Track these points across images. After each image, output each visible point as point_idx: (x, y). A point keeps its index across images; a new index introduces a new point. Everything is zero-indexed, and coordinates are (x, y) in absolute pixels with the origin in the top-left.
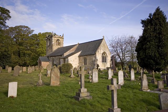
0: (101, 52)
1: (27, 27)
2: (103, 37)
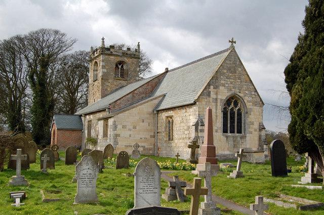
0: (219, 97)
2: (232, 42)
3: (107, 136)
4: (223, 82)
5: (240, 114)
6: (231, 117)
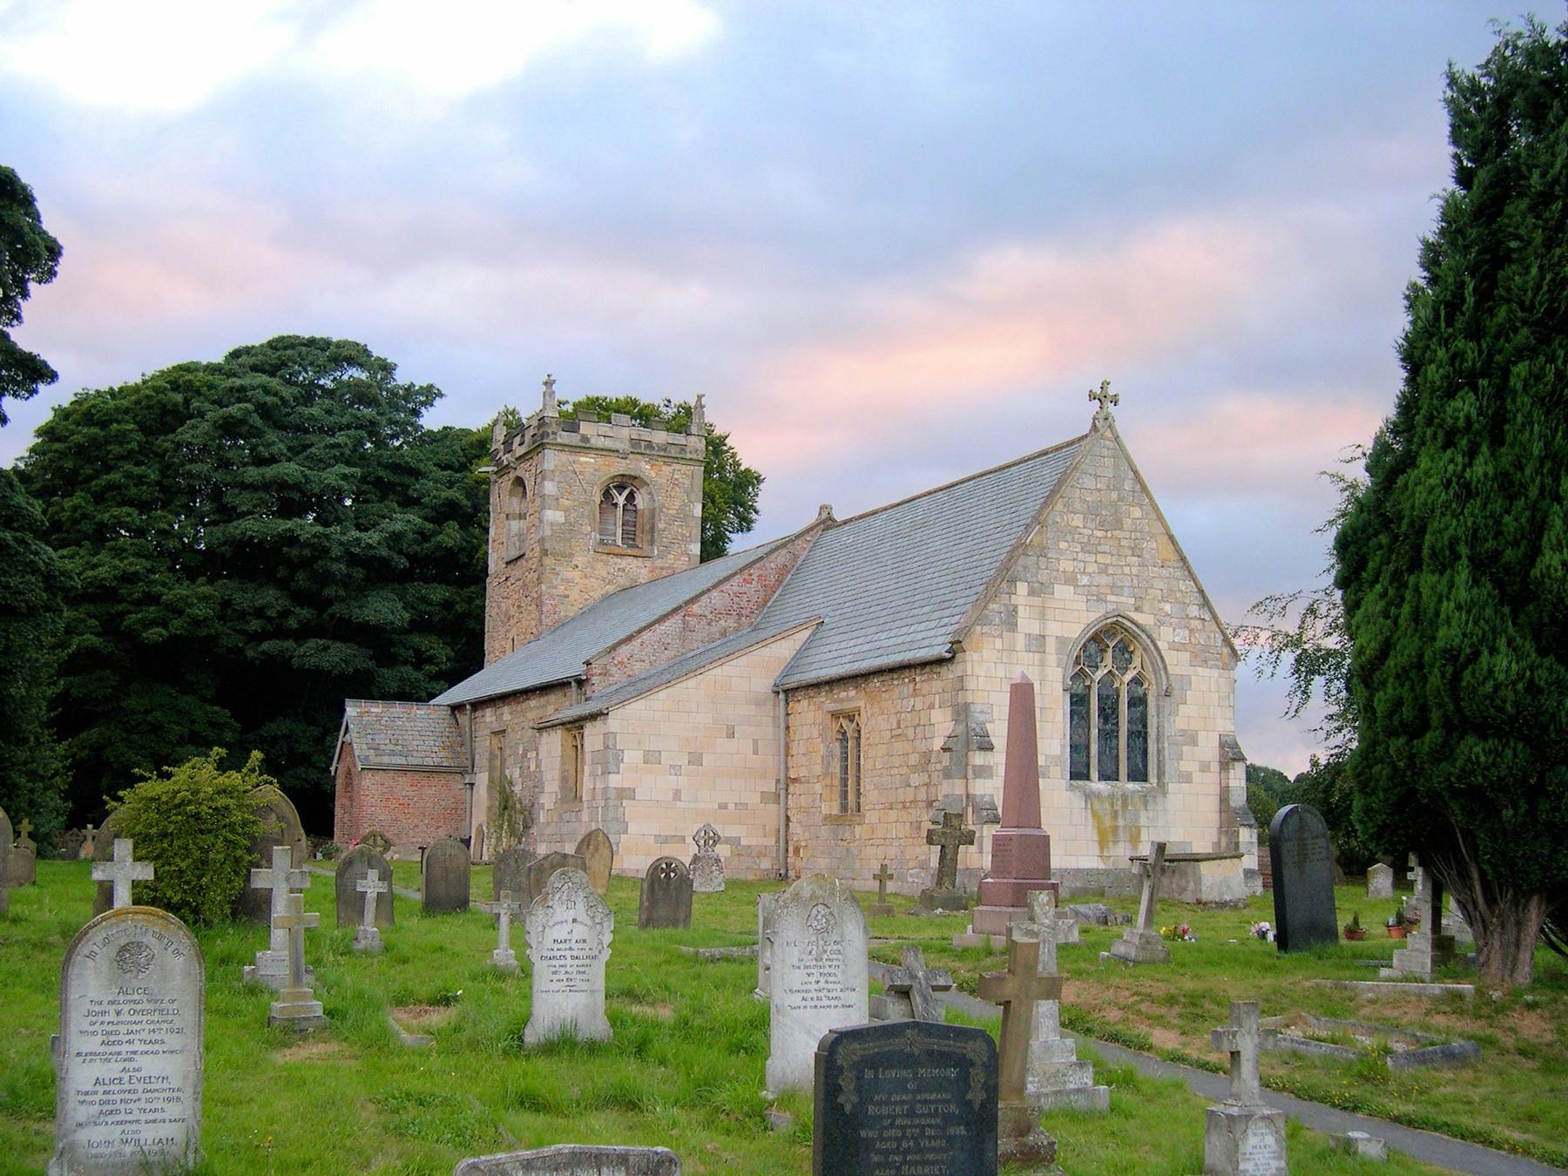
0: (1053, 629)
1: (352, 354)
2: (1102, 397)
3: (577, 798)
4: (1066, 565)
5: (1138, 702)
6: (1102, 710)
